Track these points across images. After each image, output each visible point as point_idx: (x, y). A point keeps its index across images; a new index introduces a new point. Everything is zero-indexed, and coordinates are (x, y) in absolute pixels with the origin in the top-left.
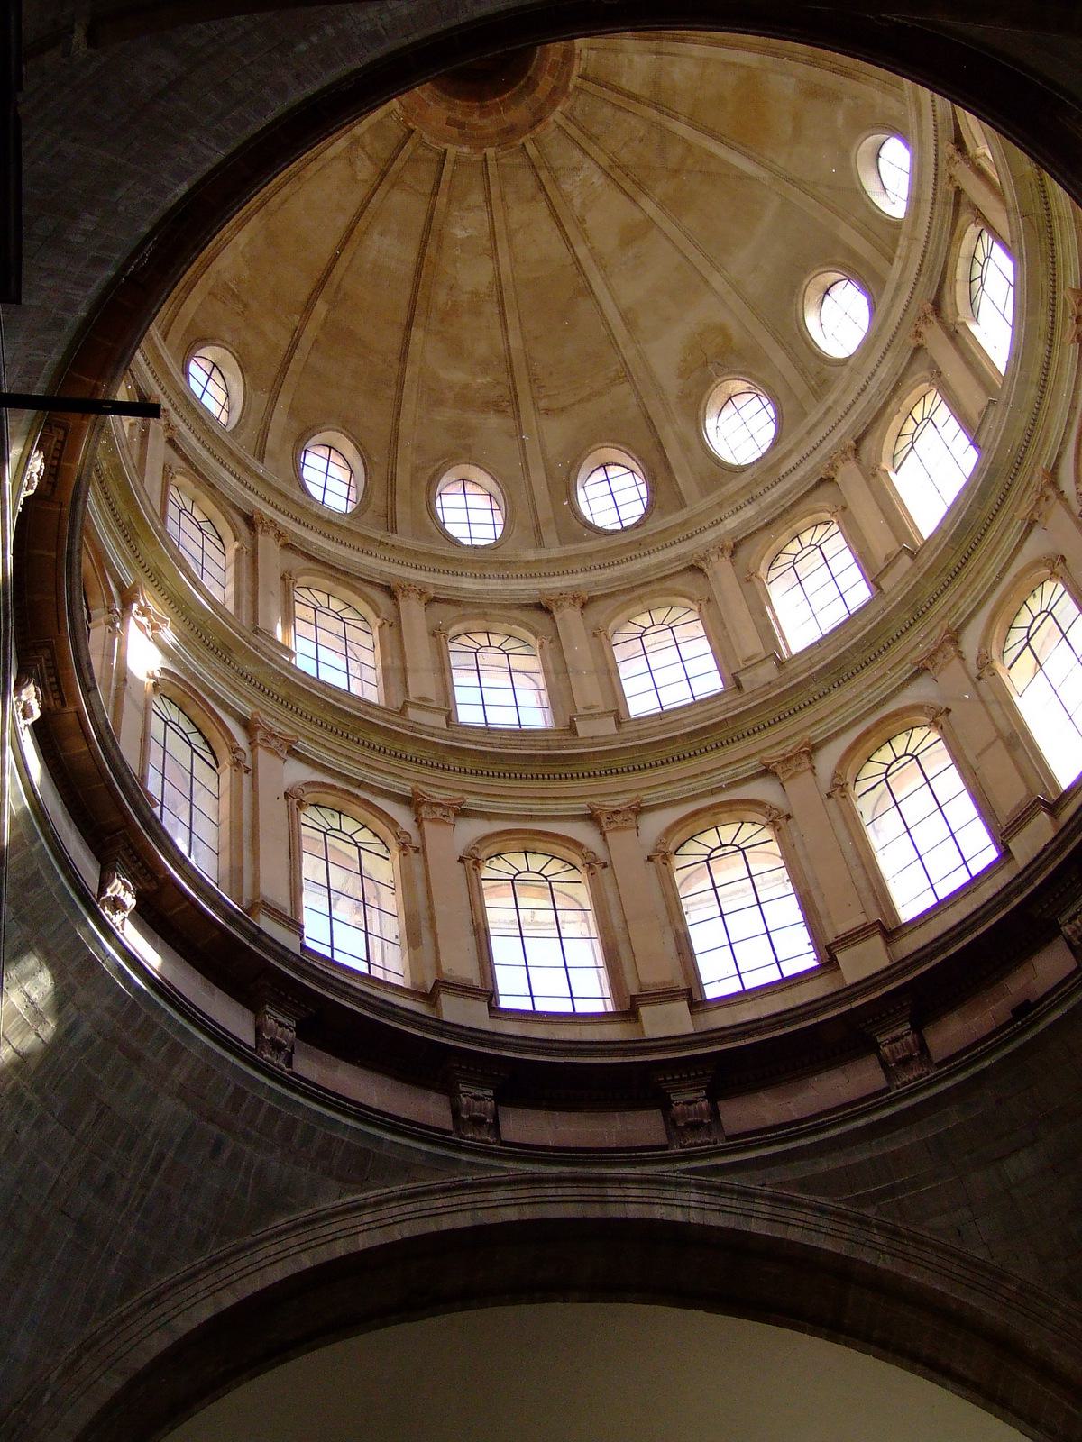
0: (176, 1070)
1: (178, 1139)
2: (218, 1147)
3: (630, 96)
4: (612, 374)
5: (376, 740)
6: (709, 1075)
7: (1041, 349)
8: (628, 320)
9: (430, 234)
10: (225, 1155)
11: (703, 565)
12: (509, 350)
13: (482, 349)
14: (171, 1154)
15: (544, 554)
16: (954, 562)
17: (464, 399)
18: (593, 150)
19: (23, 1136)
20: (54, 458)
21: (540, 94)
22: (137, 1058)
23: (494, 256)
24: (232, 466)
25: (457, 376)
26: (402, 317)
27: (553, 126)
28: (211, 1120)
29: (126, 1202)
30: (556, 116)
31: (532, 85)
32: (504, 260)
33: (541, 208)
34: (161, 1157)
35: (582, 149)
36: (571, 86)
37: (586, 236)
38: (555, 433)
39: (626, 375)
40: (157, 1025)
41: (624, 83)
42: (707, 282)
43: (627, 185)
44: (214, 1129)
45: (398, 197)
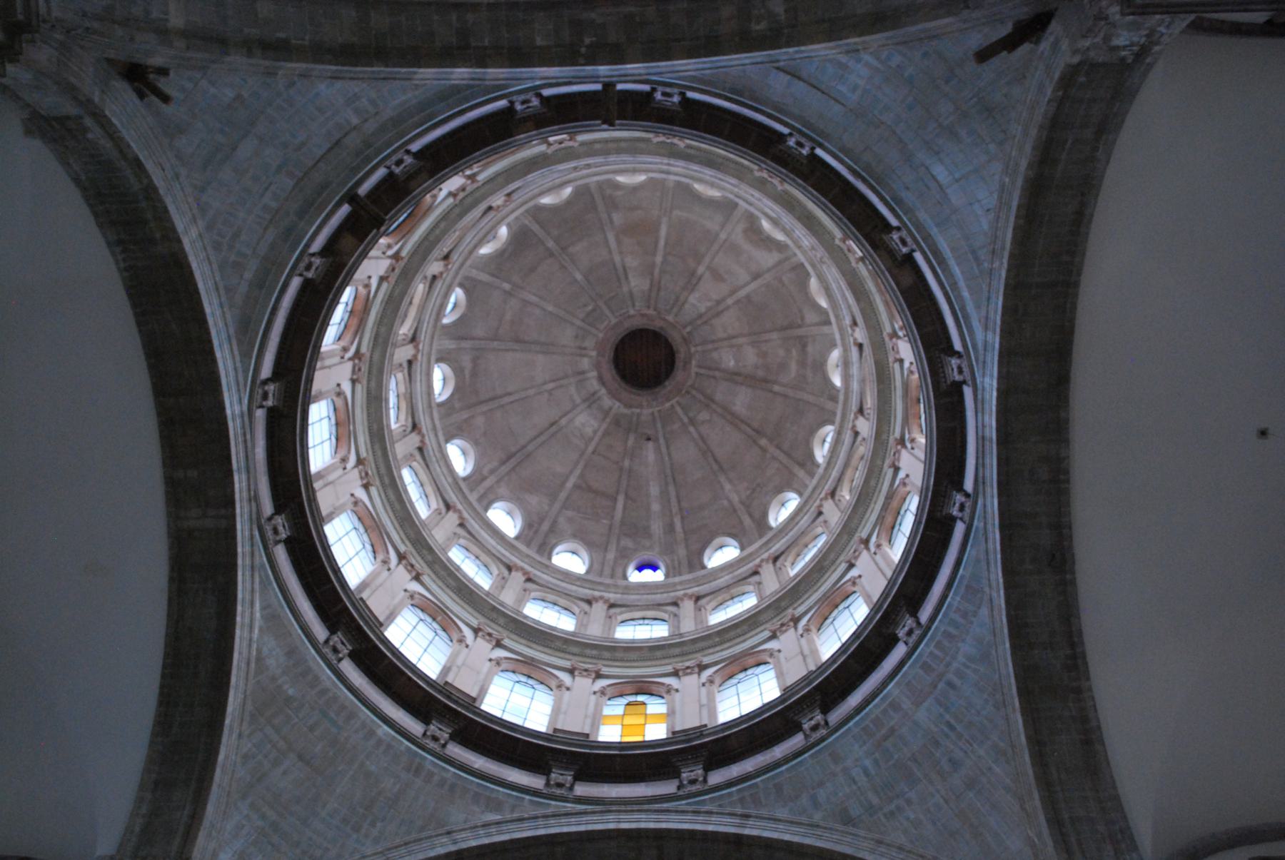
0: (904, 706)
2: (950, 684)
3: (651, 285)
9: (735, 377)
10: (957, 682)
13: (781, 352)
14: (947, 717)
18: (682, 298)
19: (912, 816)
22: (892, 731)
23: (740, 346)
24: (799, 518)
25: (793, 367)
28: (935, 687)
29: (965, 752)
30: (670, 318)
31: (661, 328)
33: (715, 322)
35: (683, 304)
37: (723, 300)
43: (694, 281)
44: (941, 685)
45: (719, 397)
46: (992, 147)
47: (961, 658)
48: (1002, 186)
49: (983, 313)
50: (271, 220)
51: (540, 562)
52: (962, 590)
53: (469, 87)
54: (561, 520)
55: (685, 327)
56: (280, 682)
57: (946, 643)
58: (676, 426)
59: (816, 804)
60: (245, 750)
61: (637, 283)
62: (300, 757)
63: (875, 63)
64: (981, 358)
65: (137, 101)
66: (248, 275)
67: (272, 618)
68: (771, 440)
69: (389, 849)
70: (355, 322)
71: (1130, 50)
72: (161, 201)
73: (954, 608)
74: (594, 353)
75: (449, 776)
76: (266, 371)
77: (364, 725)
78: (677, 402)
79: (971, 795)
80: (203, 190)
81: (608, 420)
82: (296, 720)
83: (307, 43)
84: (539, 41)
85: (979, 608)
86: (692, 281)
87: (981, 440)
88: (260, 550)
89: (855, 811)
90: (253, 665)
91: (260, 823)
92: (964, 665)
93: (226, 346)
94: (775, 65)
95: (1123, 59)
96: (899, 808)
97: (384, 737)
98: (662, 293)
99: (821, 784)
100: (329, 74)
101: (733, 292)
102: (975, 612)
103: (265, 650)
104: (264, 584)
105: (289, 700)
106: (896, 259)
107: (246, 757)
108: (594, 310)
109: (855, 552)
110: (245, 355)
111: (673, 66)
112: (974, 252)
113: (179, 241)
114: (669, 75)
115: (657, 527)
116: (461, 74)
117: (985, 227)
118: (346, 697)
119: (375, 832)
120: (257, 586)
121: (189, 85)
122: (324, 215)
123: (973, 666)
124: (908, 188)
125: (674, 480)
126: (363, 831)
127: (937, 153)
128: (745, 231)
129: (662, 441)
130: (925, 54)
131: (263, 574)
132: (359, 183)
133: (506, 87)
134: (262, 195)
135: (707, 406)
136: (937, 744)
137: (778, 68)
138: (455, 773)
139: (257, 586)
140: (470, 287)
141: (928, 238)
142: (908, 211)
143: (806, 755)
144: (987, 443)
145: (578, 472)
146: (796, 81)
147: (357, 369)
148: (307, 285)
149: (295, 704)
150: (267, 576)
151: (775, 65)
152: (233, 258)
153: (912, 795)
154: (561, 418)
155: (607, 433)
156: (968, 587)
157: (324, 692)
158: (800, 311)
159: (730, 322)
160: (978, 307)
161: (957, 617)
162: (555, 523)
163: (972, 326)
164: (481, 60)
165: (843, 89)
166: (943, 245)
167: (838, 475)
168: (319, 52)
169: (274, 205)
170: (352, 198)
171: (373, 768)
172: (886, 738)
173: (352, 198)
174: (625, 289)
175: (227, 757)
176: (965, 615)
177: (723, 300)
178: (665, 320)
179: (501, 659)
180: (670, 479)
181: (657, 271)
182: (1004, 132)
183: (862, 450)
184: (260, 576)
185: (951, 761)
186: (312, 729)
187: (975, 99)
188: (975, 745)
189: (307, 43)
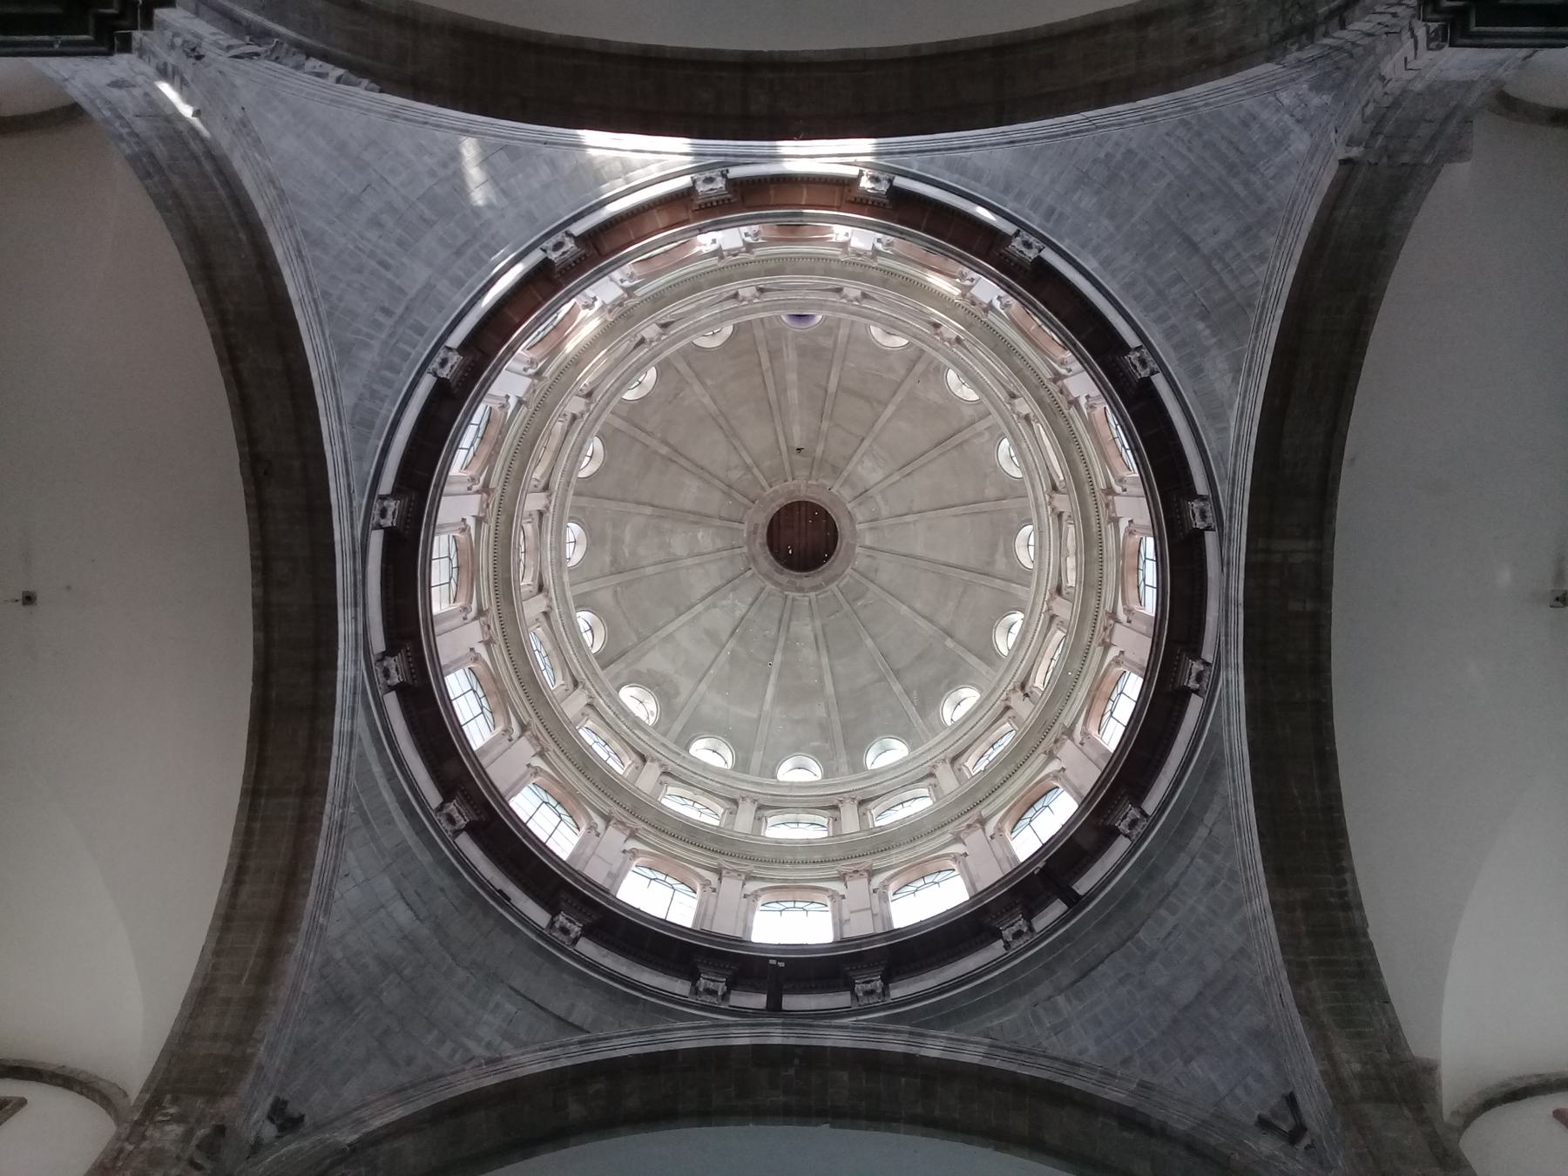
1: (398, 282)
2: (387, 312)
4: (640, 630)
5: (516, 465)
6: (413, 681)
7: (817, 857)
8: (669, 638)
9: (697, 518)
10: (380, 317)
11: (580, 686)
12: (642, 567)
13: (642, 551)
14: (389, 275)
15: (567, 587)
16: (668, 828)
17: (618, 541)
20: (879, 203)
21: (777, 577)
22: (459, 253)
23: (691, 555)
24: (616, 385)
26: (656, 502)
27: (762, 585)
28: (407, 308)
30: (770, 586)
32: (689, 562)
33: (719, 582)
34: (387, 267)
36: (786, 593)
37: (708, 609)
38: (605, 597)
39: (643, 639)
40: (479, 268)
41: (794, 623)
42: (700, 681)
44: (399, 310)
45: (717, 496)
46: (338, 955)
47: (376, 344)
48: (327, 912)
49: (355, 752)
50: (1168, 895)
51: (923, 341)
52: (378, 423)
53: (927, 1025)
54: (903, 372)
55: (753, 575)
56: (1214, 340)
57: (396, 360)
58: (767, 463)
60: (1264, 268)
61: (804, 628)
62: (1194, 247)
63: (471, 1044)
64: (359, 698)
65: (1298, 1096)
66: (1202, 832)
67: (1217, 415)
68: (655, 452)
69: (1088, 130)
70: (1106, 687)
71: (166, 1115)
72: (1287, 962)
73: (388, 401)
74: (858, 550)
75: (1011, 204)
76: (1196, 703)
77: (1113, 274)
78: (765, 491)
79: (351, 191)
80: (1242, 951)
81: (845, 474)
82: (1196, 292)
83: (1101, 1119)
84: (845, 1076)
85: (356, 405)
86: (739, 628)
87: (360, 600)
88: (1223, 497)
90: (1244, 366)
91: (1253, 178)
92: (371, 337)
93: (1237, 755)
94: (584, 1036)
95: (175, 1101)
97: (1090, 257)
98: (777, 615)
100: (1082, 1071)
101: (697, 617)
102: (360, 399)
103: (1228, 378)
104: (1221, 456)
105: (1204, 316)
106: (462, 791)
107: (1262, 258)
108: (856, 600)
109: (534, 391)
110: (1215, 736)
111: (699, 1038)
112: (366, 822)
113: (1273, 904)
114: (703, 1023)
115: (790, 356)
116: (933, 1048)
117: (350, 855)
118: (1131, 308)
119: (1108, 147)
120: (1231, 460)
121: (1239, 1091)
122: (1109, 888)
123: (361, 337)
124: (442, 890)
125: (770, 407)
126: (1123, 149)
127: (405, 937)
128: (678, 693)
129: (783, 447)
130: (410, 1061)
131: (1223, 471)
132: (1063, 920)
133: (888, 1019)
134: (1175, 927)
135: (730, 486)
136: (401, 243)
137: (580, 1029)
138: (1005, 206)
139: (1231, 460)
140: (988, 654)
141: (421, 831)
142: (442, 861)
143: (566, 218)
144: (350, 599)
145: (883, 419)
146: (562, 1015)
147: (1108, 632)
148: (1138, 798)
149: (1197, 311)
150: (1218, 468)
151: (584, 1036)
152: (1218, 858)
153: (428, 182)
154: (899, 481)
155: (849, 459)
156: (371, 426)
157: (1161, 319)
158: (618, 602)
159: (700, 582)
160: (362, 756)
161: (383, 390)
162: (910, 370)
163: (371, 732)
164: (910, 1064)
165: (510, 1008)
166: (402, 825)
167: (569, 437)
168: (1087, 1104)
169: (1163, 912)
170: (1075, 902)
171: (1106, 222)
172: (467, 244)
173: (1075, 902)
174: (818, 623)
175: (1286, 267)
176: (374, 394)
177: (708, 609)
178: (777, 584)
179: (756, 891)
180: (775, 407)
181: (781, 644)
182: (323, 977)
183: (538, 473)
184: (1226, 469)
186: (1179, 279)
187: (356, 1011)
188: (351, 247)
189: (1101, 1119)
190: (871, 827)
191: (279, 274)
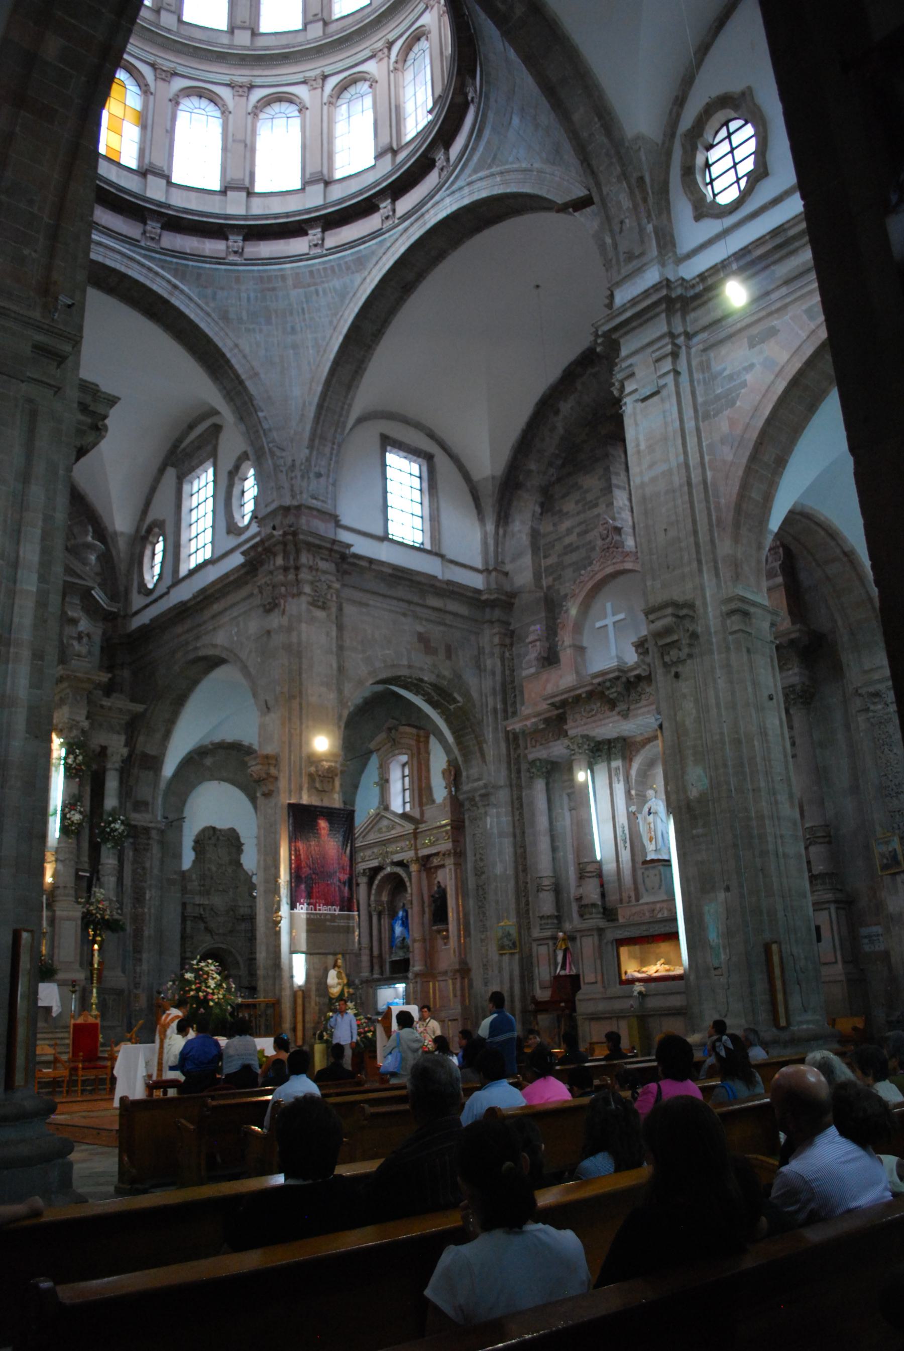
1: (304, 300)
2: (317, 292)
10: (321, 293)
22: (274, 289)
34: (303, 310)
44: (313, 288)
57: (329, 272)
59: (214, 298)
64: (454, 188)
79: (291, 351)
89: (232, 316)
96: (254, 330)
99: (222, 289)
136: (291, 313)
172: (269, 290)
176: (348, 268)
185: (293, 328)
190: (39, 1036)
191: (335, 358)
